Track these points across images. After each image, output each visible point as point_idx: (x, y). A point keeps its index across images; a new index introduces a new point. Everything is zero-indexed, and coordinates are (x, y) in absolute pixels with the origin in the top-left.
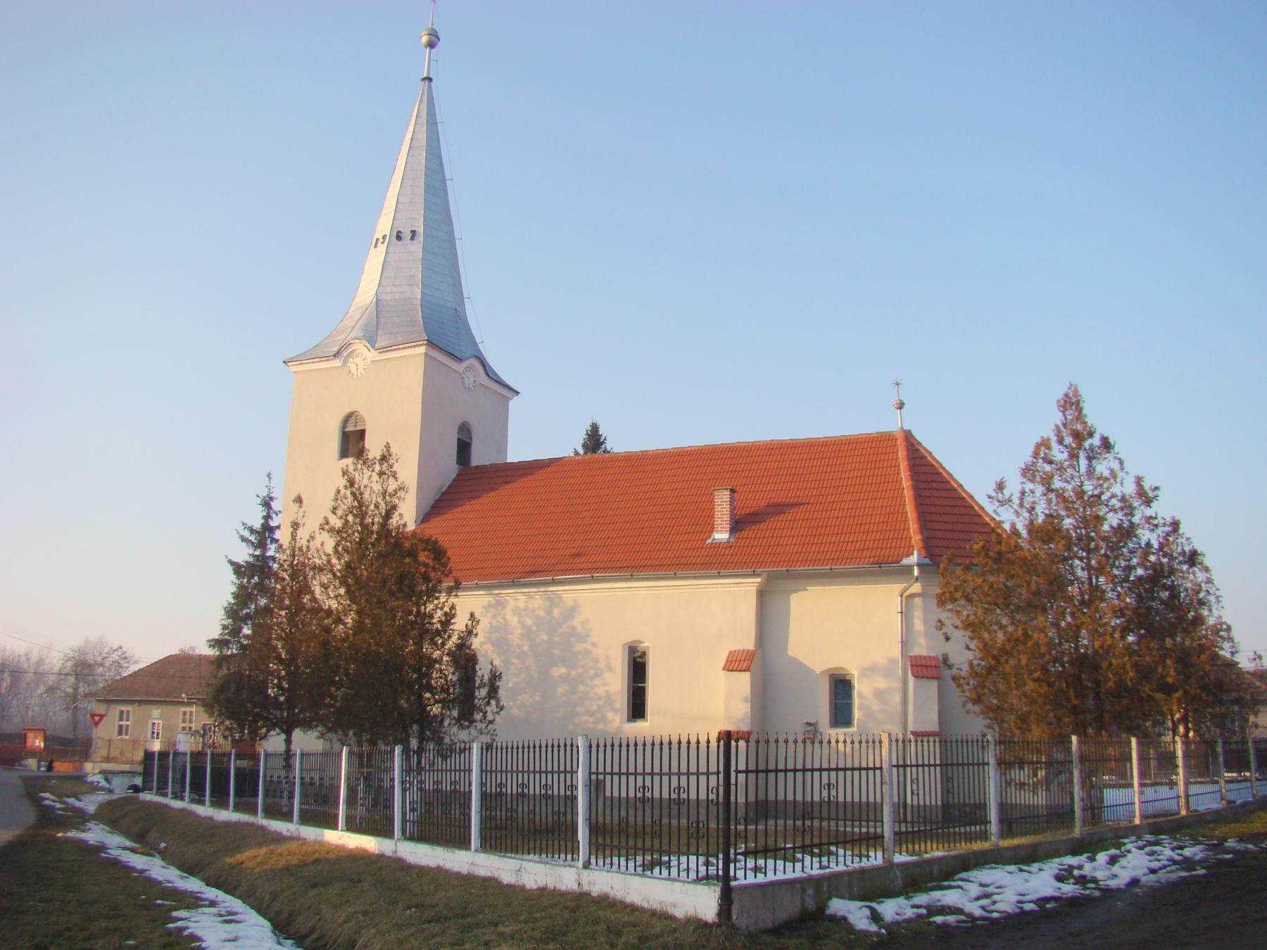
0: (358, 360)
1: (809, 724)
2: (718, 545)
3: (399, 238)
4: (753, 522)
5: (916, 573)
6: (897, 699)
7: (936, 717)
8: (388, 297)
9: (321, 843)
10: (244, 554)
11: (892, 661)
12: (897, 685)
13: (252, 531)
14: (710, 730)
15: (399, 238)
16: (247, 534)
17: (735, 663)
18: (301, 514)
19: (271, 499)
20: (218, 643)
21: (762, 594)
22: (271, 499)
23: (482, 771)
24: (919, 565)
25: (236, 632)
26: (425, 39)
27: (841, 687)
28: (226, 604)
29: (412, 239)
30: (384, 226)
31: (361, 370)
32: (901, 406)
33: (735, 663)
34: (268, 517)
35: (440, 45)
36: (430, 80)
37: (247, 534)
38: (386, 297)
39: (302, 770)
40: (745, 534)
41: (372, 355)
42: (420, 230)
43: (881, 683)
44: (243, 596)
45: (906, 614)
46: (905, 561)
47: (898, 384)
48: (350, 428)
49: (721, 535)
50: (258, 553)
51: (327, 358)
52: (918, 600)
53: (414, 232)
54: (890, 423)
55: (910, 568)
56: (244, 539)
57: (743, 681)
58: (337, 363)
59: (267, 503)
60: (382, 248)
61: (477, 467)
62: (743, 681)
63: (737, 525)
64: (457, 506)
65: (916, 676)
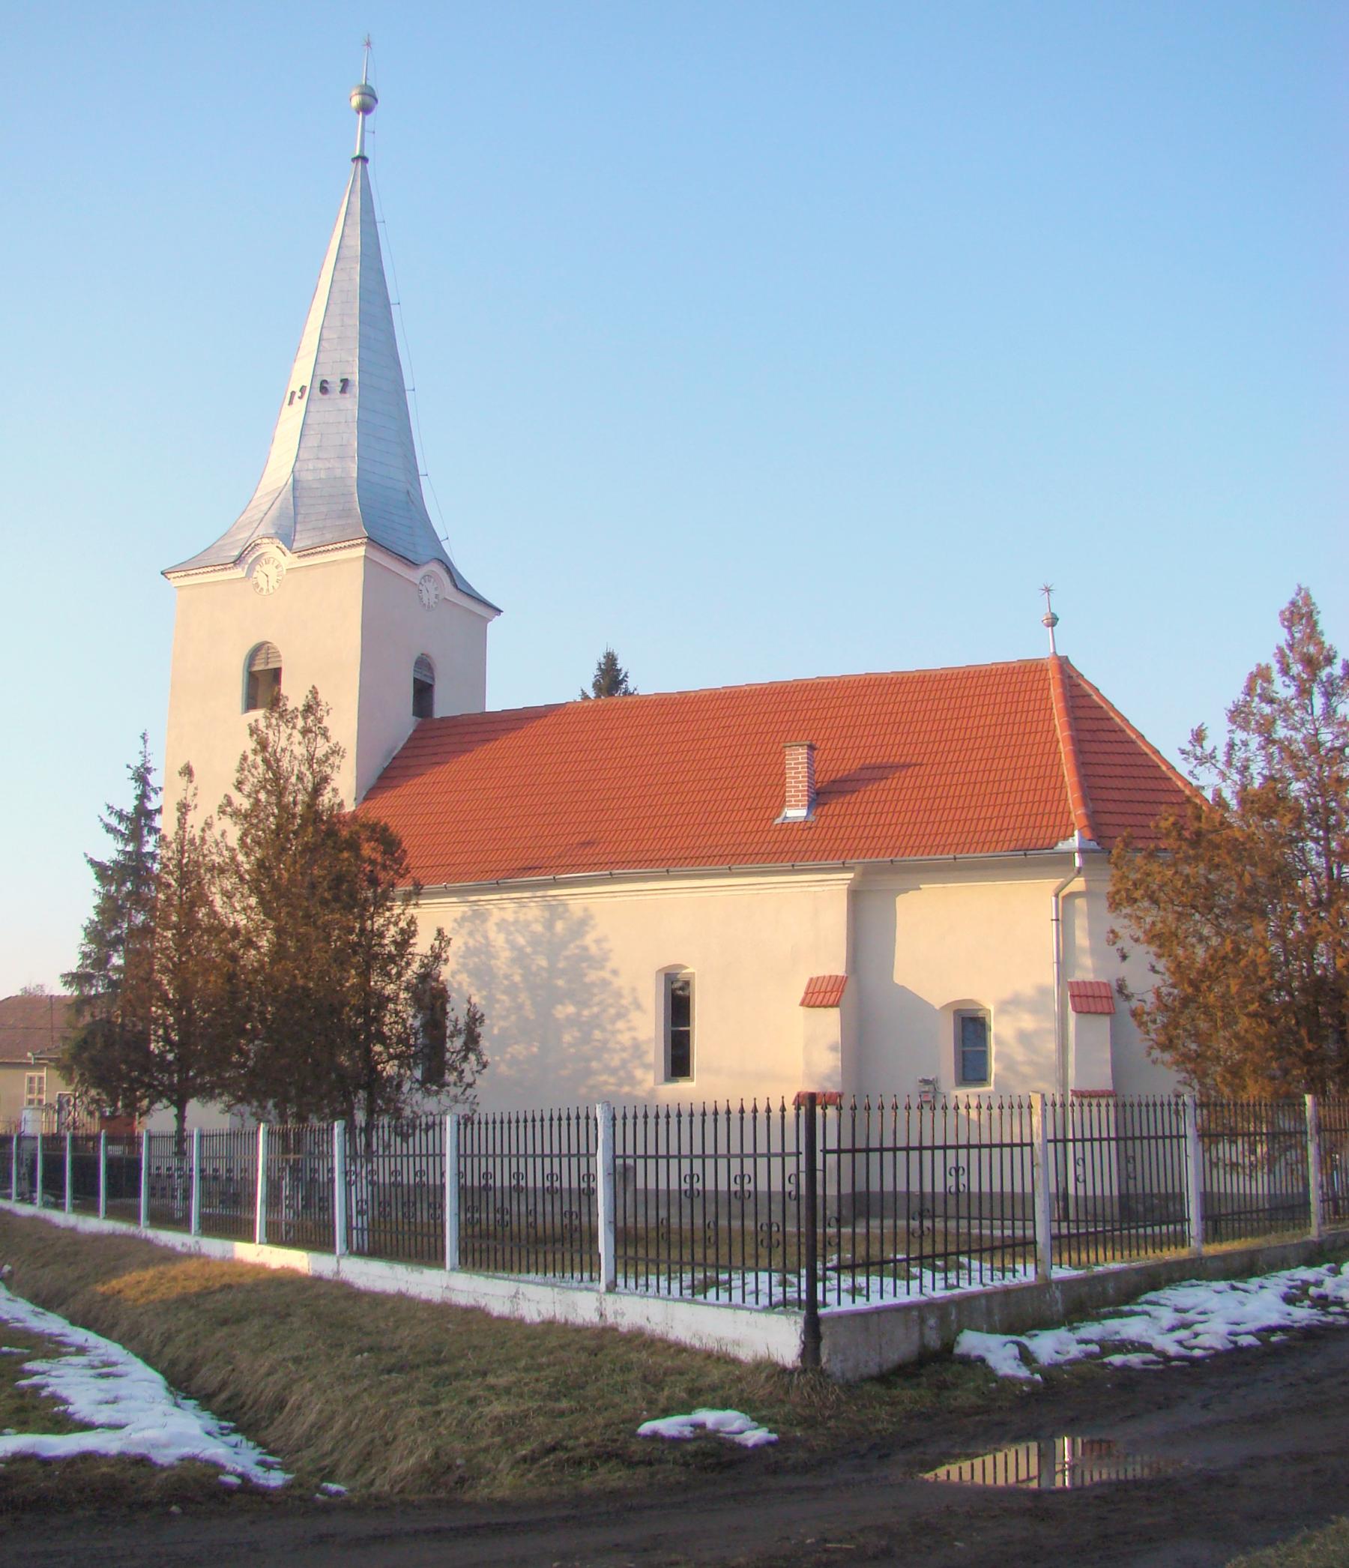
0: (269, 569)
1: (926, 1082)
2: (792, 826)
3: (324, 389)
4: (842, 793)
5: (1077, 862)
6: (1051, 1045)
8: (310, 476)
10: (110, 850)
11: (1043, 991)
15: (324, 389)
16: (114, 821)
17: (818, 995)
19: (148, 770)
21: (855, 895)
24: (1081, 851)
26: (356, 101)
27: (971, 1027)
28: (86, 923)
29: (343, 391)
31: (273, 582)
32: (1053, 621)
34: (143, 797)
35: (379, 109)
37: (114, 821)
38: (306, 476)
39: (201, 1158)
40: (835, 807)
41: (289, 560)
42: (355, 378)
44: (110, 911)
45: (1064, 921)
49: (796, 812)
50: (130, 848)
51: (224, 566)
56: (110, 829)
57: (830, 1021)
58: (239, 572)
60: (300, 405)
62: (830, 1021)
63: (819, 796)
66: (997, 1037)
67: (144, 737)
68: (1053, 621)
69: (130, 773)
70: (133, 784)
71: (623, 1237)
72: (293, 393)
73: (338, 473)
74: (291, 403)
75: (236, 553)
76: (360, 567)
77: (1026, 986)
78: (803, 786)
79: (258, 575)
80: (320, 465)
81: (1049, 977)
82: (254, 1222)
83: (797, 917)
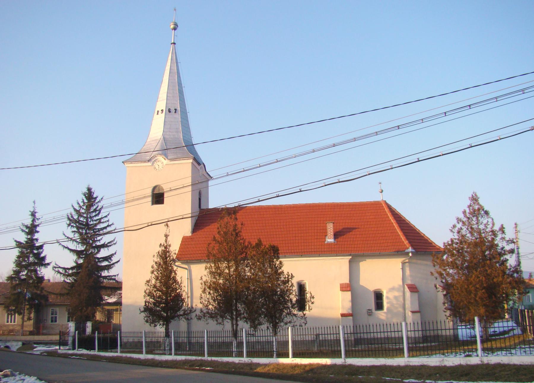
0: (159, 163)
1: (369, 310)
2: (329, 244)
3: (170, 111)
4: (341, 235)
5: (410, 254)
6: (401, 299)
7: (418, 306)
8: (168, 137)
9: (278, 364)
10: (23, 238)
11: (400, 285)
12: (401, 294)
13: (27, 227)
14: (337, 314)
15: (170, 111)
16: (25, 229)
17: (344, 288)
18: (168, 231)
19: (36, 213)
20: (10, 278)
21: (350, 262)
22: (36, 213)
23: (339, 334)
24: (412, 252)
25: (17, 273)
26: (172, 27)
27: (379, 296)
28: (14, 261)
29: (175, 112)
30: (161, 105)
31: (160, 167)
32: (382, 192)
33: (344, 288)
34: (34, 221)
35: (178, 29)
36: (175, 44)
37: (25, 229)
38: (166, 136)
39: (207, 337)
40: (340, 239)
41: (166, 162)
42: (179, 109)
43: (396, 294)
44: (22, 256)
45: (403, 269)
46: (406, 251)
47: (380, 183)
48: (156, 192)
49: (330, 240)
50: (29, 237)
51: (145, 162)
52: (407, 264)
53: (176, 110)
54: (378, 198)
55: (408, 253)
56: (23, 231)
57: (348, 295)
58: (150, 164)
59: (33, 214)
60: (162, 116)
61: (215, 209)
62: (348, 295)
63: (336, 235)
64: (206, 226)
65: (411, 291)
66: (387, 298)
67: (34, 202)
68: (382, 192)
69: (30, 213)
70: (30, 217)
71: (346, 351)
72: (158, 111)
73: (176, 136)
74: (158, 114)
75: (148, 158)
76: (190, 165)
77: (396, 286)
78: (332, 233)
79: (156, 165)
80: (171, 134)
81: (401, 283)
82: (340, 351)
83: (336, 267)
